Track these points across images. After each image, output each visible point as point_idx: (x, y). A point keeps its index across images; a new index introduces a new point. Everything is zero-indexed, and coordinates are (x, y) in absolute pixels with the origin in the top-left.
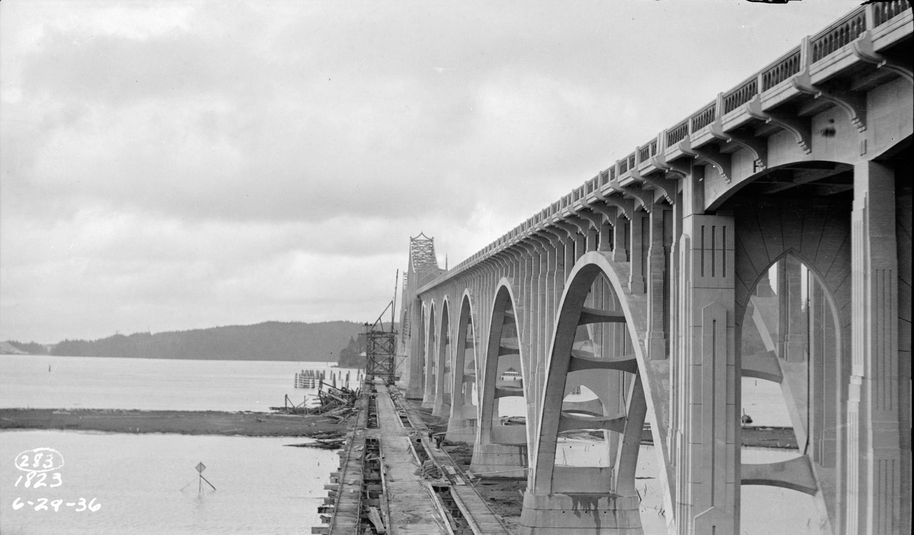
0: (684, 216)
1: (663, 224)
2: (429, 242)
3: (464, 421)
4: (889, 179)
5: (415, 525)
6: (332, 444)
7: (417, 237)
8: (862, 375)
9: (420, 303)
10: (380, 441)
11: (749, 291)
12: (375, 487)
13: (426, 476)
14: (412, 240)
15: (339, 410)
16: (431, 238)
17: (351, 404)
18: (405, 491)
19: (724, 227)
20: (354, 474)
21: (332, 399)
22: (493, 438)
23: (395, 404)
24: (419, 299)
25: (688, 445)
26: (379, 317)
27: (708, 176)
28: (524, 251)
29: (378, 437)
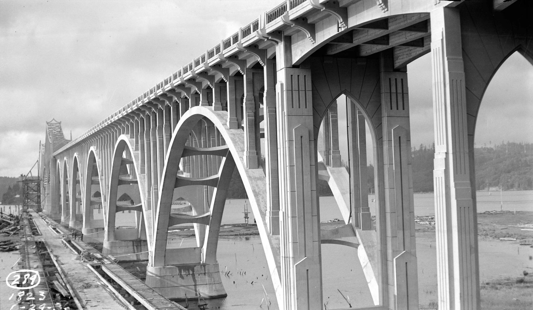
0: (277, 70)
1: (253, 81)
2: (58, 125)
3: (92, 230)
4: (456, 20)
5: (89, 290)
6: (8, 248)
7: (51, 121)
8: (446, 151)
9: (55, 161)
10: (44, 243)
11: (321, 118)
12: (50, 269)
13: (84, 260)
14: (48, 123)
15: (9, 228)
16: (59, 122)
17: (17, 224)
18: (73, 270)
19: (305, 76)
20: (35, 262)
21: (4, 222)
22: (116, 238)
23: (46, 222)
24: (55, 159)
25: (288, 219)
26: (29, 171)
27: (350, 13)
28: (124, 123)
29: (43, 240)
